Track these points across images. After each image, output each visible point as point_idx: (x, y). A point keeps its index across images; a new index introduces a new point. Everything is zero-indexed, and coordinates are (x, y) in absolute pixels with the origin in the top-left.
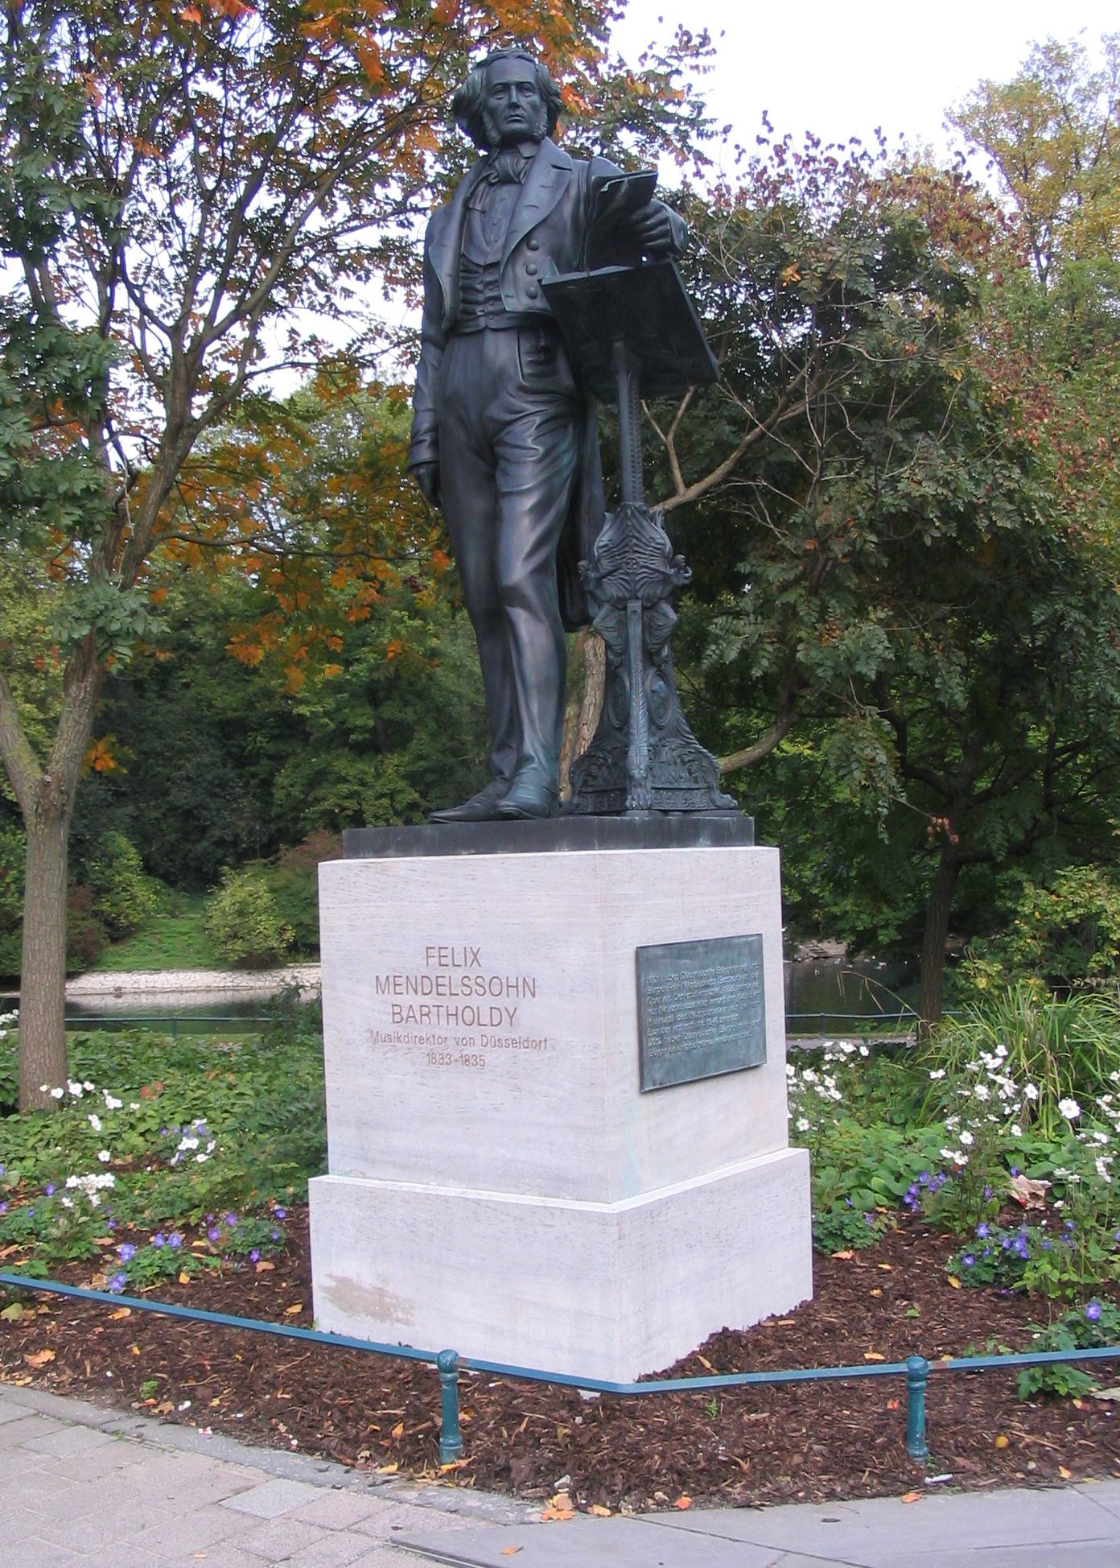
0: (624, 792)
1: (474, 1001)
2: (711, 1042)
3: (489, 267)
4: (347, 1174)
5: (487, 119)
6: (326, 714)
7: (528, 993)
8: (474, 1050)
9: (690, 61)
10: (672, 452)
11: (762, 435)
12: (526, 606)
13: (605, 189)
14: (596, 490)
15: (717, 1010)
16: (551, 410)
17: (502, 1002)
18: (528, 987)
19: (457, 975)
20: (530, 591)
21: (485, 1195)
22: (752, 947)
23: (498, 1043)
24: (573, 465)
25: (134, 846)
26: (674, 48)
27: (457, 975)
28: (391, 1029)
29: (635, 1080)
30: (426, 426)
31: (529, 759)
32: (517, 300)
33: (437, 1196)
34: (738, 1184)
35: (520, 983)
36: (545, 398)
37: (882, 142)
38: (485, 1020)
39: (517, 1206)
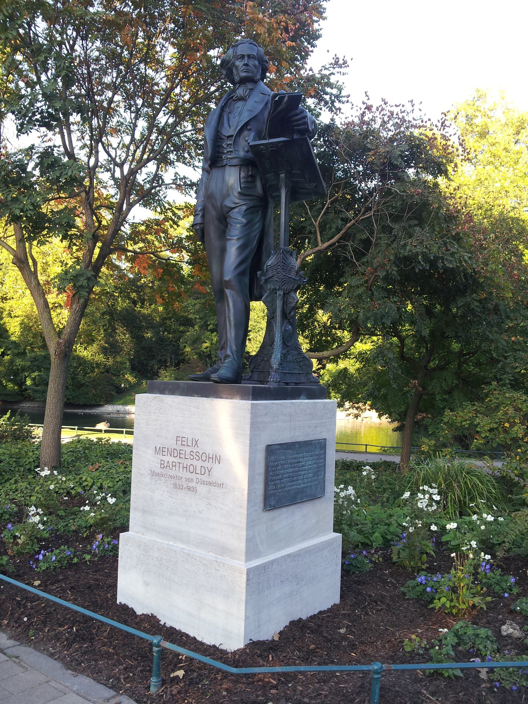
1: (195, 462)
2: (299, 487)
7: (217, 462)
8: (193, 484)
9: (337, 69)
11: (354, 224)
13: (277, 99)
15: (303, 472)
16: (252, 204)
17: (205, 464)
19: (188, 450)
20: (234, 283)
23: (203, 483)
24: (259, 229)
26: (331, 64)
27: (188, 450)
28: (159, 470)
34: (308, 551)
36: (247, 198)
37: (413, 106)
38: (198, 471)
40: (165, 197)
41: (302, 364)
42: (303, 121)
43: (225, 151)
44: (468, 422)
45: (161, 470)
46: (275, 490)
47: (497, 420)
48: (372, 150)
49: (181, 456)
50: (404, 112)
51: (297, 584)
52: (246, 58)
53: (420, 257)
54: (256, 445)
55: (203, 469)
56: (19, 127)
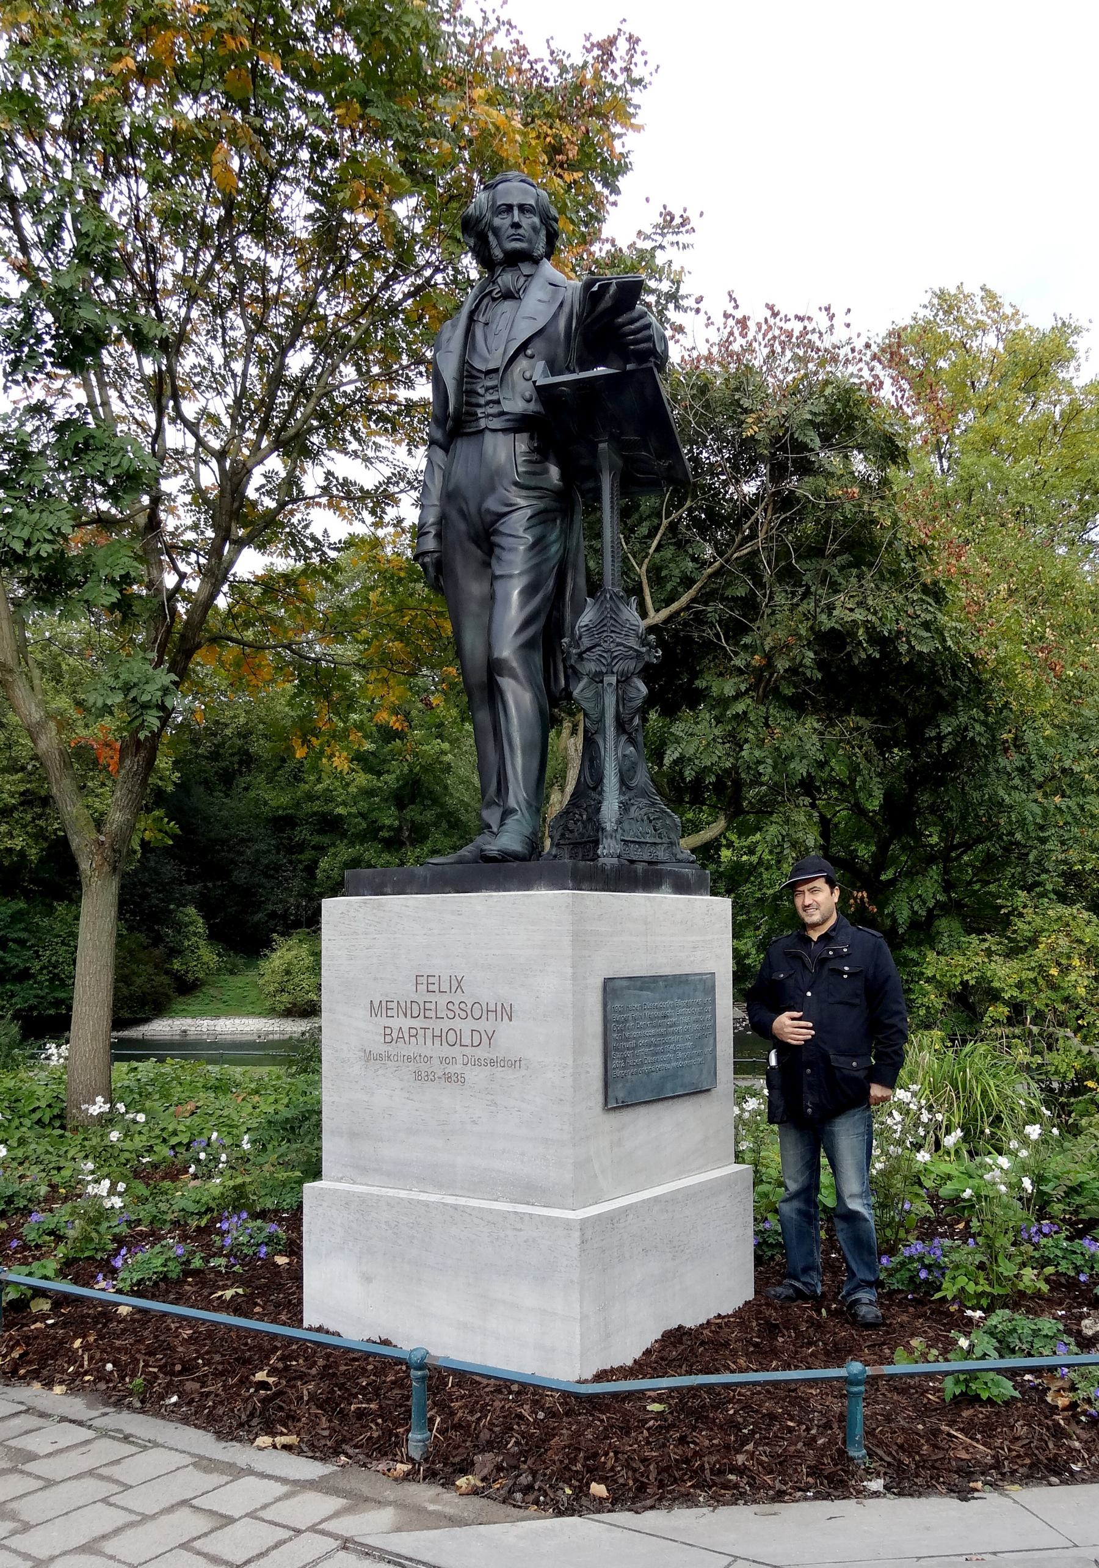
0: (596, 843)
1: (457, 1024)
2: (668, 1066)
3: (488, 373)
4: (340, 1180)
5: (491, 238)
6: (361, 815)
7: (505, 1017)
8: (457, 1068)
9: (671, 238)
10: (645, 581)
11: (722, 566)
12: (515, 677)
13: (595, 288)
14: (576, 582)
16: (541, 505)
17: (483, 1025)
18: (506, 1012)
19: (443, 1000)
21: (462, 1201)
22: (706, 984)
23: (478, 1062)
25: (203, 917)
27: (443, 1000)
28: (383, 1049)
29: (600, 1098)
30: (431, 520)
31: (513, 811)
32: (516, 402)
33: (419, 1201)
35: (499, 1009)
36: (536, 494)
37: (832, 318)
38: (466, 1040)
39: (490, 1211)
40: (306, 527)
41: (659, 824)
42: (645, 333)
43: (482, 401)
44: (975, 974)
45: (385, 1047)
46: (624, 1068)
47: (1033, 964)
48: (752, 411)
49: (428, 1014)
50: (813, 331)
51: (674, 1258)
52: (516, 212)
53: (861, 631)
54: (585, 978)
55: (476, 1035)
56: (8, 370)
